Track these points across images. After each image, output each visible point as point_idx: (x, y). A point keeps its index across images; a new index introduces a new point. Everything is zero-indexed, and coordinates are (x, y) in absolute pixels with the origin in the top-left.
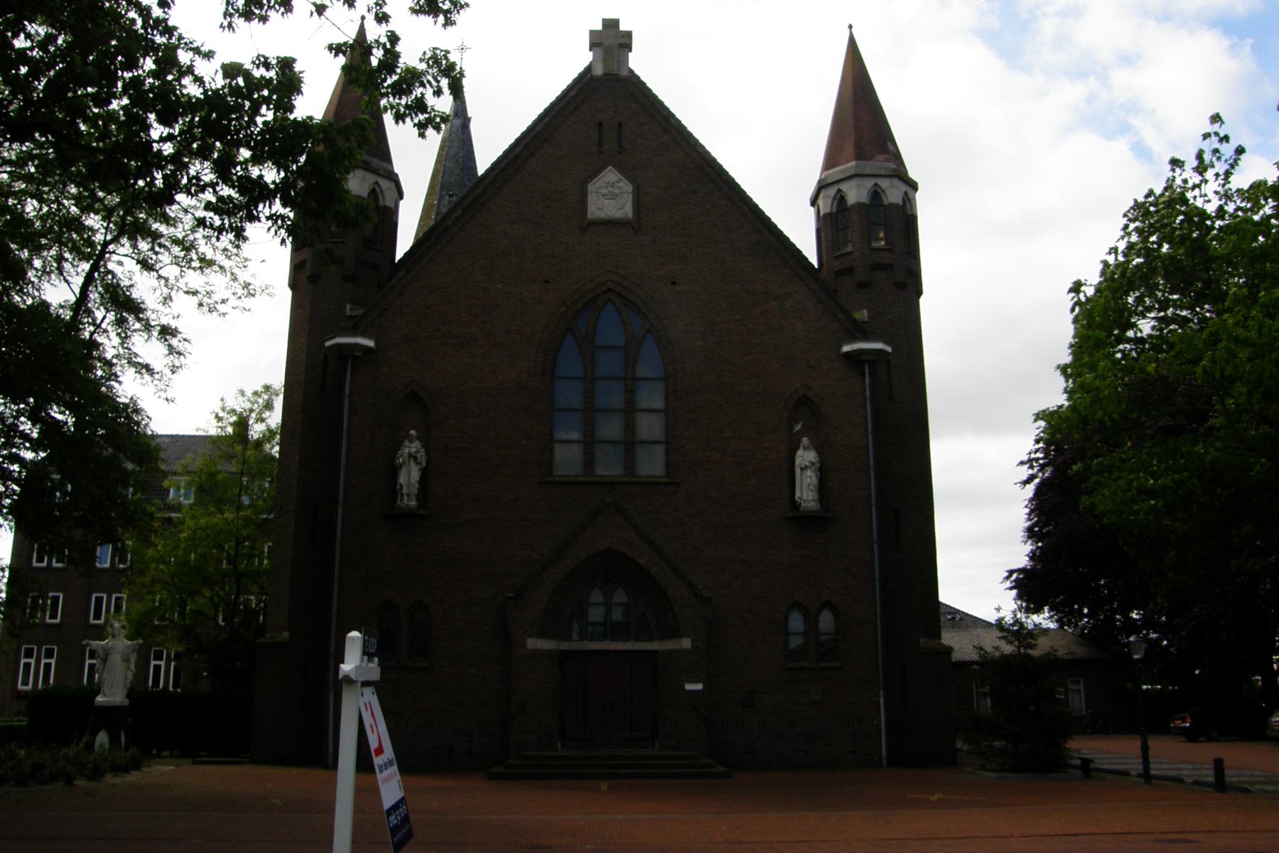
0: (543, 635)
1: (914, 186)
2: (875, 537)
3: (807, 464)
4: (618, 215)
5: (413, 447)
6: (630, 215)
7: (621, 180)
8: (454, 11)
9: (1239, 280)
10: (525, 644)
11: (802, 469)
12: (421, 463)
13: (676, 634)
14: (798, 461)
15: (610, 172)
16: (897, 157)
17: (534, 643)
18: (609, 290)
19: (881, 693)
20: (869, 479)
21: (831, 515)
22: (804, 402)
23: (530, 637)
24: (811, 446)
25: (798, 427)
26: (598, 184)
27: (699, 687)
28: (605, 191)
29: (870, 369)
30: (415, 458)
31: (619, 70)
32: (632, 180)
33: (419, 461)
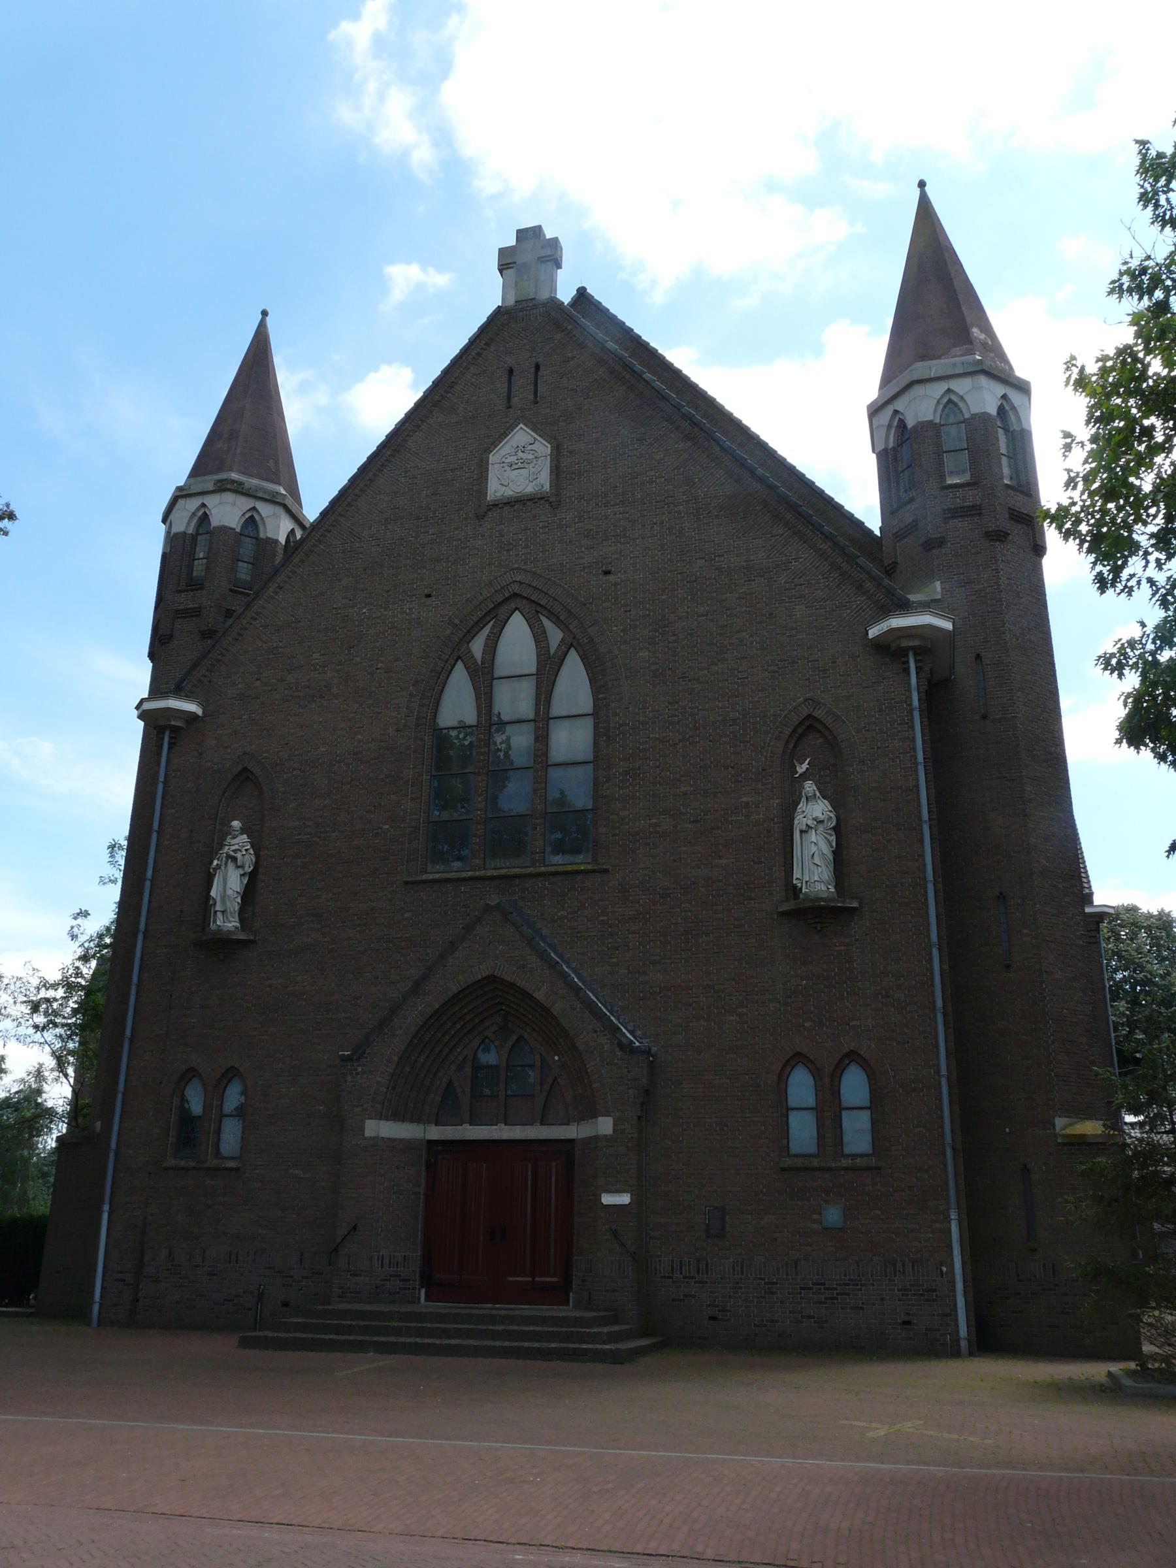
0: (397, 1116)
1: (1023, 388)
2: (934, 937)
3: (810, 822)
4: (530, 489)
5: (239, 843)
6: (547, 487)
7: (535, 439)
10: (362, 1129)
11: (801, 832)
12: (242, 867)
13: (591, 1113)
14: (800, 821)
16: (994, 348)
18: (515, 595)
19: (953, 1215)
20: (921, 841)
21: (855, 904)
22: (809, 726)
24: (818, 794)
25: (802, 768)
26: (503, 452)
27: (625, 1199)
28: (513, 459)
29: (916, 661)
30: (235, 859)
31: (536, 293)
32: (552, 438)
33: (239, 864)
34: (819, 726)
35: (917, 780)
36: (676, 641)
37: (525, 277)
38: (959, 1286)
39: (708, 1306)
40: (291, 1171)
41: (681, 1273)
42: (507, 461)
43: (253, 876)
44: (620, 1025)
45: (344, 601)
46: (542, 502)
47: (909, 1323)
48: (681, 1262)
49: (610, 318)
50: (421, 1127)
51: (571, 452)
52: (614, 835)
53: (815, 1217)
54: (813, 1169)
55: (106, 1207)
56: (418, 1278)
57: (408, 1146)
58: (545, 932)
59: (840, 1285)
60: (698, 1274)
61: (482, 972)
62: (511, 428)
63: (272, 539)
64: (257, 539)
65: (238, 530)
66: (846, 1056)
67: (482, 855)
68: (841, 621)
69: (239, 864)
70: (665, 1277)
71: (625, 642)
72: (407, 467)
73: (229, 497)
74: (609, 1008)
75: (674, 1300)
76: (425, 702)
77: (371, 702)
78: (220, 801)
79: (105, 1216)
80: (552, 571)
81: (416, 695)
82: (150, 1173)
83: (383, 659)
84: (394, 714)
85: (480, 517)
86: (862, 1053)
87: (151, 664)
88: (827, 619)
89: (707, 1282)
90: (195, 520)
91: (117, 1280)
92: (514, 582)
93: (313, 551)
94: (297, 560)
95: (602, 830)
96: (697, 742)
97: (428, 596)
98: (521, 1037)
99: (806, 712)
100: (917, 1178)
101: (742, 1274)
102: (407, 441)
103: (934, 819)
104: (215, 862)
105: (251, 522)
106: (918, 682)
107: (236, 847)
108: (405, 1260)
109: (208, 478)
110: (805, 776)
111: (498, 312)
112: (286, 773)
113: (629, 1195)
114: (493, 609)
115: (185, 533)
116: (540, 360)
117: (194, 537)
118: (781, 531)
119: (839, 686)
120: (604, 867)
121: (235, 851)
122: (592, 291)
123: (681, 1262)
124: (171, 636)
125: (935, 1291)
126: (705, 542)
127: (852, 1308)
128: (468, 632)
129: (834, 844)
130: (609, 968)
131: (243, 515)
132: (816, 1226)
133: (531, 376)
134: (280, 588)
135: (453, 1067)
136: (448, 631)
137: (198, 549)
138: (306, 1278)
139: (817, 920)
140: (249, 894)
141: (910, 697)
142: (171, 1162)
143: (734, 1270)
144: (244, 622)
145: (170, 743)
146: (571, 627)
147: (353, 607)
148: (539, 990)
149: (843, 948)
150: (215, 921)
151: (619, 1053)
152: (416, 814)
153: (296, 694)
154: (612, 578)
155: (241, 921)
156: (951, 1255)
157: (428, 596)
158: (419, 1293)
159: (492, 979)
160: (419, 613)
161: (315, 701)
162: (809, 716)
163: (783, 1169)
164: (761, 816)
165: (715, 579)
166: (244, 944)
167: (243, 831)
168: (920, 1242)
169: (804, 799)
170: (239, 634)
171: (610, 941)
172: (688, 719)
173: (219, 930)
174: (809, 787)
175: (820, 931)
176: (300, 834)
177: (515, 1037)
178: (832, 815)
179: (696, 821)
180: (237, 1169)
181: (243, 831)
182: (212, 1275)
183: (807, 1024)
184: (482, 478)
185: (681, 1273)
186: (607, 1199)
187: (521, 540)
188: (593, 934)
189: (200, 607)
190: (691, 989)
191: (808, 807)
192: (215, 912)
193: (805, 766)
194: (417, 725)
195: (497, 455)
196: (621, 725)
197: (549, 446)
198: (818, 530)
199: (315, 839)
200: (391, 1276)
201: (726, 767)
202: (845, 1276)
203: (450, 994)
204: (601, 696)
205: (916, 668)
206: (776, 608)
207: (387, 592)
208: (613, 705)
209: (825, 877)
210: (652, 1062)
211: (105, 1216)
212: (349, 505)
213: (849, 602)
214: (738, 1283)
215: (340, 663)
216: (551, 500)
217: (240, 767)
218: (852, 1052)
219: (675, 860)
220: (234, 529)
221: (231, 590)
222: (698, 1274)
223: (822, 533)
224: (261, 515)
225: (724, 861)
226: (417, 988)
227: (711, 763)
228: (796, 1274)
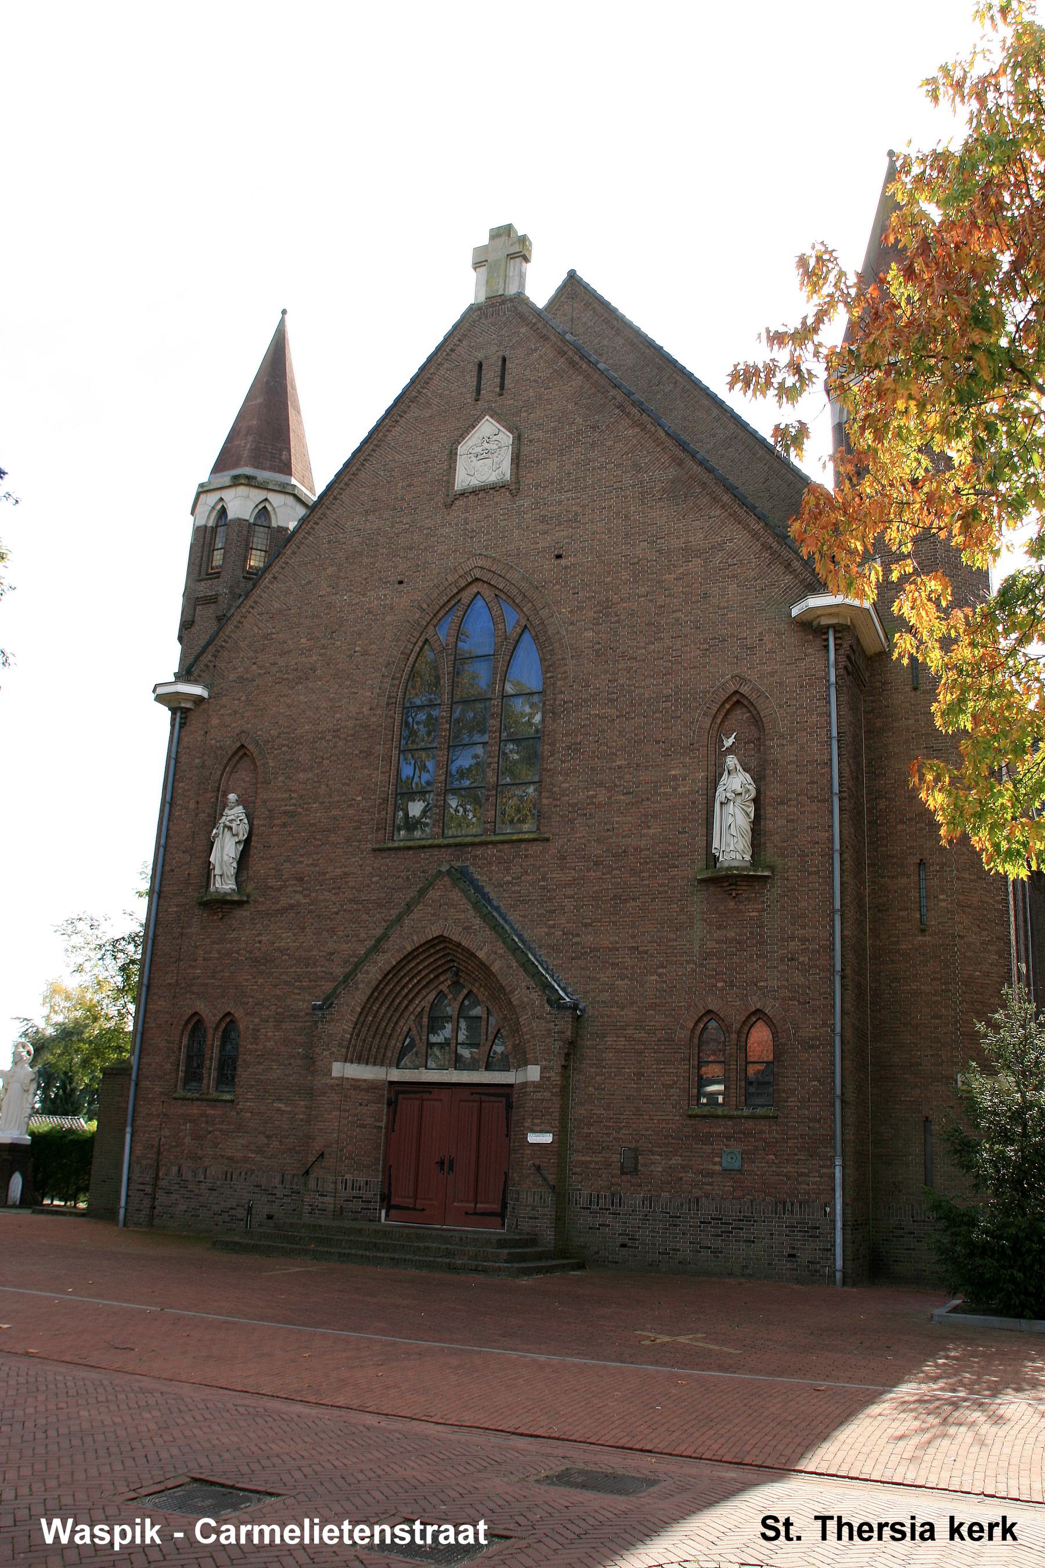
0: (360, 1059)
3: (728, 795)
4: (492, 478)
5: (235, 814)
6: (508, 477)
8: (1013, 201)
9: (53, 1092)
10: (330, 1070)
11: (722, 803)
14: (720, 795)
15: (487, 422)
17: (341, 1070)
18: (477, 580)
19: (838, 1161)
20: (831, 812)
22: (737, 701)
23: (336, 1061)
24: (739, 767)
25: (729, 742)
26: (470, 443)
27: (547, 1138)
28: (479, 450)
30: (230, 828)
33: (234, 832)
34: (746, 702)
35: (831, 753)
36: (618, 622)
37: (495, 274)
38: (839, 1225)
39: (620, 1234)
40: (275, 1105)
41: (598, 1205)
42: (473, 452)
43: (247, 842)
44: (553, 982)
45: (328, 589)
46: (503, 490)
47: (794, 1256)
48: (598, 1195)
49: (597, 298)
50: (384, 1069)
51: (531, 441)
52: (556, 806)
53: (717, 1159)
54: (717, 1117)
55: (129, 1130)
56: (379, 1200)
57: (372, 1086)
58: (492, 895)
59: (735, 1220)
60: (613, 1206)
61: (434, 931)
62: (478, 420)
63: (282, 527)
64: (269, 527)
65: (252, 521)
66: (754, 1013)
67: (441, 825)
68: (770, 599)
69: (234, 832)
70: (584, 1208)
71: (572, 624)
72: (386, 461)
73: (242, 490)
74: (545, 966)
75: (590, 1228)
76: (397, 682)
77: (348, 683)
78: (222, 775)
79: (128, 1137)
80: (509, 556)
81: (387, 676)
82: (163, 1102)
83: (360, 642)
84: (369, 694)
85: (449, 506)
86: (767, 1012)
87: (180, 647)
88: (756, 597)
89: (619, 1214)
90: (215, 513)
91: (138, 1190)
92: (476, 567)
93: (303, 543)
94: (289, 552)
95: (545, 801)
96: (632, 718)
97: (401, 582)
98: (470, 992)
99: (733, 688)
100: (809, 1127)
101: (651, 1208)
102: (386, 436)
103: (844, 792)
104: (215, 831)
105: (263, 512)
106: (836, 659)
107: (232, 817)
108: (367, 1184)
109: (225, 473)
110: (730, 750)
111: (471, 309)
112: (276, 749)
113: (551, 1135)
114: (457, 593)
115: (206, 526)
116: (507, 354)
117: (214, 530)
118: (718, 513)
119: (764, 663)
120: (546, 835)
121: (231, 821)
122: (580, 273)
123: (598, 1195)
124: (193, 622)
125: (818, 1228)
126: (649, 525)
127: (745, 1241)
128: (435, 615)
129: (752, 815)
130: (546, 930)
131: (256, 506)
132: (718, 1168)
133: (499, 369)
134: (275, 578)
135: (412, 1017)
136: (417, 615)
137: (217, 539)
138: (287, 1196)
139: (732, 887)
140: (243, 860)
141: (828, 674)
142: (180, 1093)
143: (643, 1203)
144: (244, 610)
145: (181, 723)
146: (525, 609)
147: (336, 594)
148: (481, 949)
149: (755, 914)
150: (214, 884)
151: (548, 1008)
152: (385, 787)
153: (286, 676)
154: (563, 562)
155: (237, 883)
156: (834, 1198)
157: (401, 582)
158: (380, 1213)
159: (441, 939)
160: (392, 598)
161: (302, 683)
162: (736, 692)
163: (690, 1116)
164: (687, 788)
165: (656, 561)
166: (240, 904)
167: (238, 803)
168: (808, 1185)
169: (726, 773)
170: (239, 622)
171: (548, 904)
172: (625, 696)
173: (217, 891)
174: (731, 761)
175: (734, 897)
176: (286, 805)
177: (465, 991)
178: (750, 787)
179: (628, 793)
180: (232, 1101)
181: (238, 803)
182: (212, 1190)
183: (719, 985)
184: (452, 469)
185: (598, 1205)
186: (533, 1138)
187: (483, 527)
188: (534, 898)
189: (217, 595)
190: (618, 951)
191: (730, 780)
192: (215, 876)
193: (731, 740)
194: (388, 704)
195: (464, 447)
196: (565, 702)
197: (511, 436)
198: (752, 511)
199: (299, 810)
200: (354, 1197)
201: (658, 742)
202: (740, 1212)
203: (405, 952)
204: (549, 675)
205: (836, 645)
206: (710, 588)
207: (365, 579)
208: (559, 683)
209: (740, 847)
210: (579, 1017)
211: (128, 1137)
212: (335, 498)
213: (777, 581)
214: (646, 1216)
215: (324, 647)
216: (511, 488)
217: (238, 745)
218: (758, 1010)
219: (608, 830)
220: (247, 521)
221: (244, 577)
222: (613, 1206)
223: (754, 514)
224: (272, 506)
225: (652, 831)
226: (376, 947)
227: (645, 737)
228: (698, 1210)
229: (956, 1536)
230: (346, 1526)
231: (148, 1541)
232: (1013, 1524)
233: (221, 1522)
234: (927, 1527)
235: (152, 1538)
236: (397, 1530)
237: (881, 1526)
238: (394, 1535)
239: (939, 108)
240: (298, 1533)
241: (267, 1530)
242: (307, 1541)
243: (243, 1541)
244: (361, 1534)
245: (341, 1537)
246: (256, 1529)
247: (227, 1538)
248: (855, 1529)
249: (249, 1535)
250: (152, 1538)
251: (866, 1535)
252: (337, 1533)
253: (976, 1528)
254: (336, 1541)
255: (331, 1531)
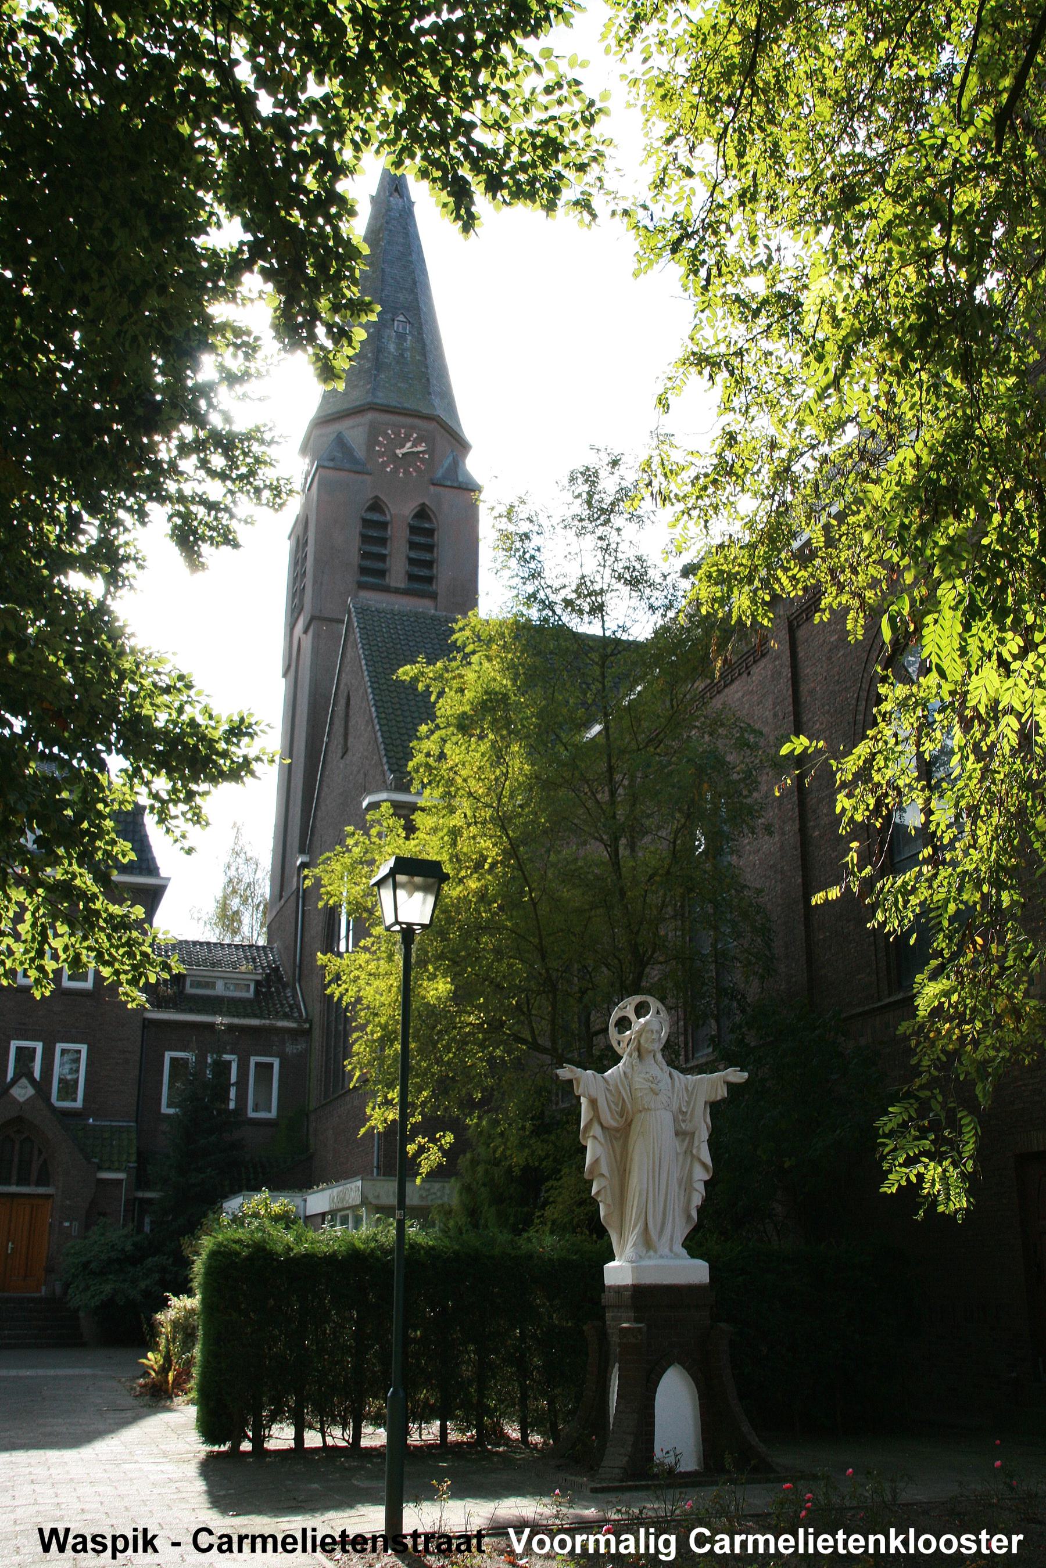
5: (784, 750)
229: (150, 1549)
230: (841, 1536)
231: (892, 1551)
232: (154, 1537)
233: (715, 1532)
234: (80, 1539)
235: (897, 1548)
236: (963, 1539)
237: (241, 1539)
238: (960, 1545)
239: (613, 113)
240: (792, 1543)
241: (761, 1539)
242: (801, 1550)
243: (737, 1550)
244: (855, 1544)
245: (835, 1547)
246: (751, 1538)
247: (722, 1547)
248: (318, 1542)
249: (744, 1544)
250: (897, 1548)
251: (289, 1547)
252: (831, 1543)
253: (290, 1540)
254: (830, 1550)
255: (825, 1540)
